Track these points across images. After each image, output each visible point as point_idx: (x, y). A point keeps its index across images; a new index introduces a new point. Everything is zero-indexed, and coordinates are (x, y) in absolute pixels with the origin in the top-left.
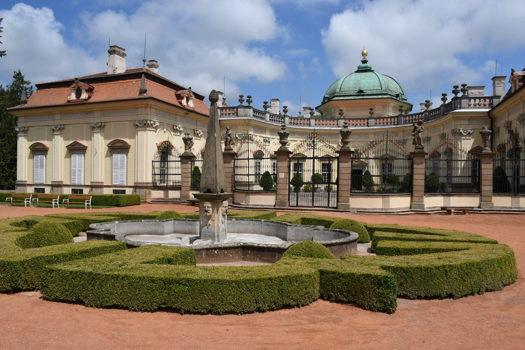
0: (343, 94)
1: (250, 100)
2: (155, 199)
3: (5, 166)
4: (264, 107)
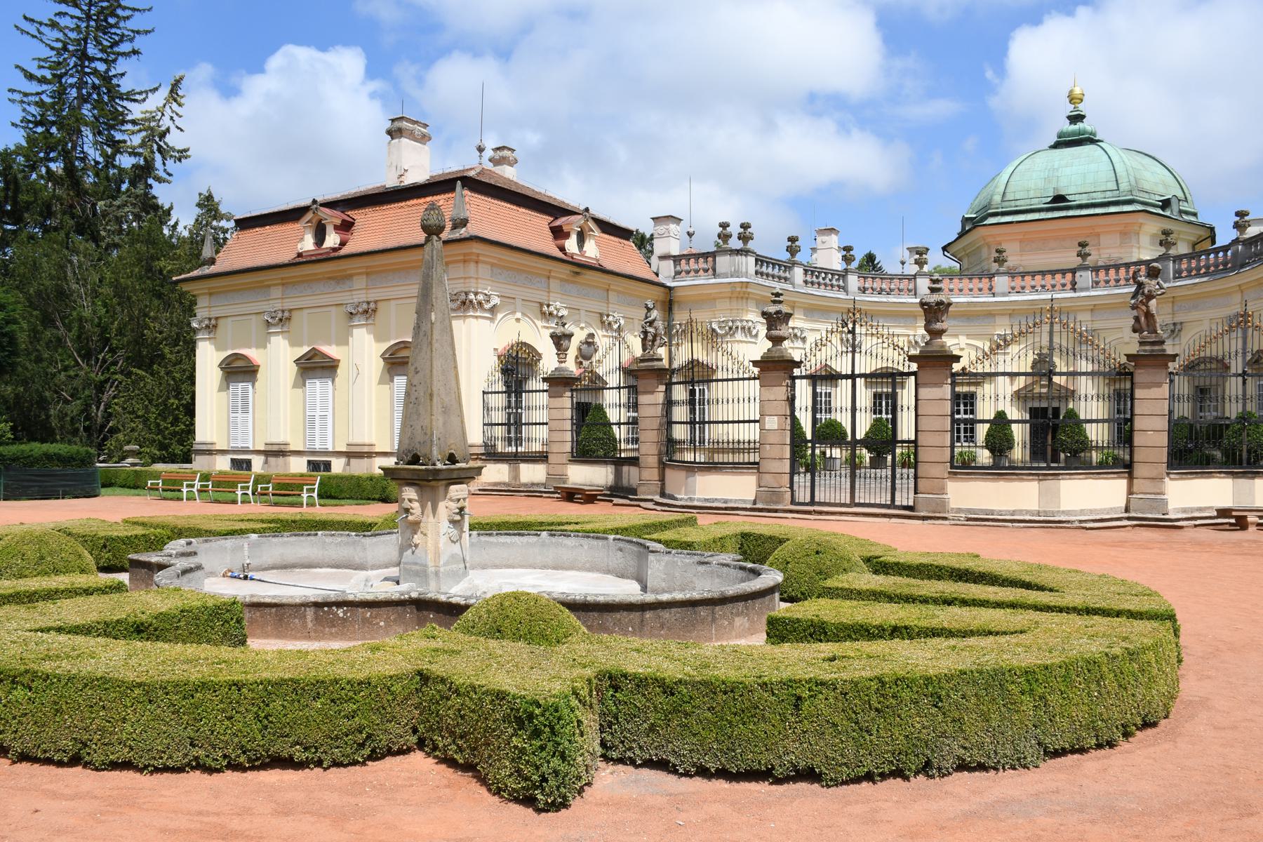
0: (1011, 207)
1: (747, 233)
2: (490, 484)
3: (178, 408)
4: (789, 249)
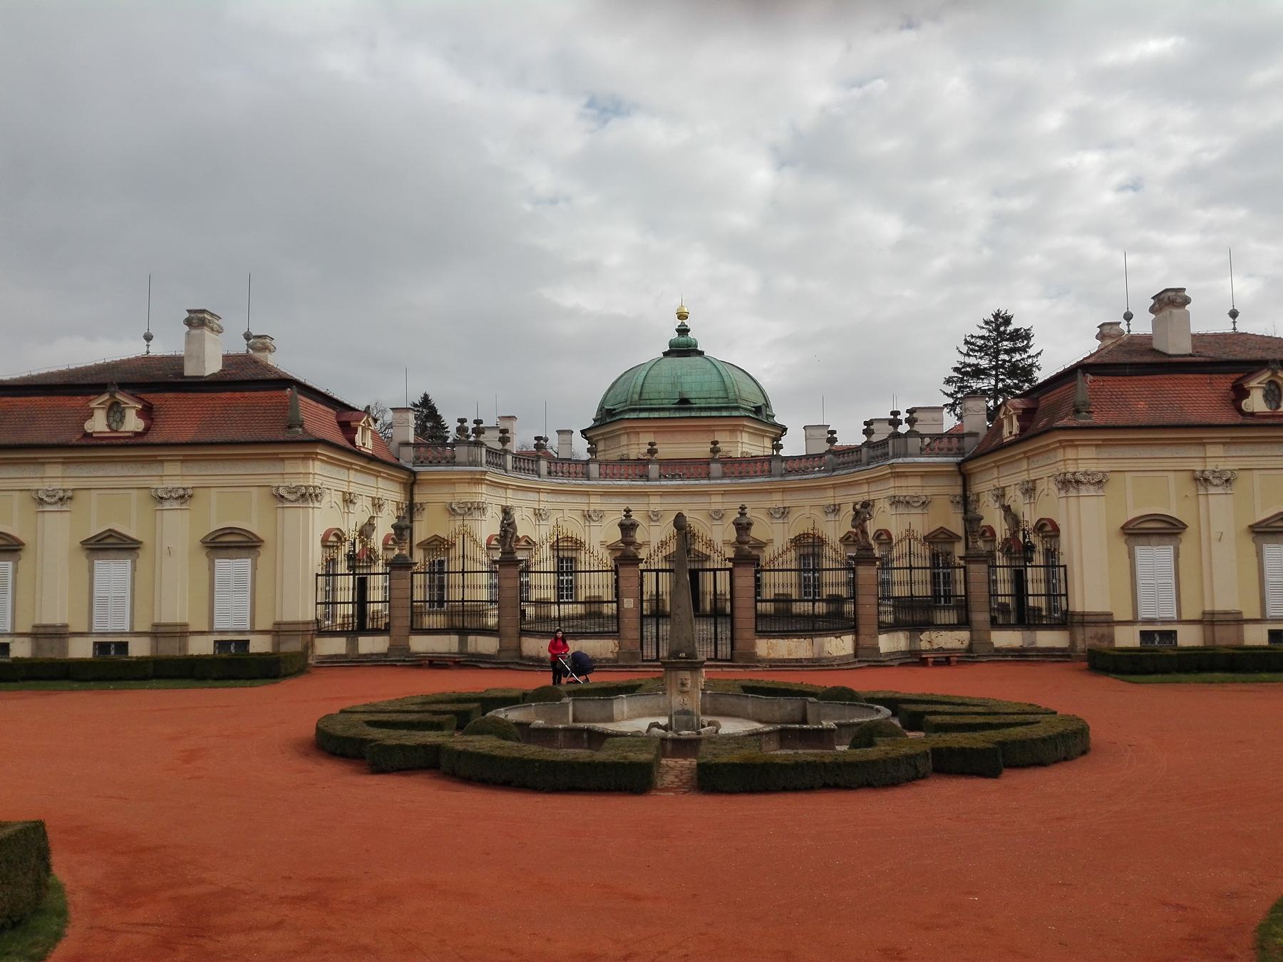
0: (647, 405)
